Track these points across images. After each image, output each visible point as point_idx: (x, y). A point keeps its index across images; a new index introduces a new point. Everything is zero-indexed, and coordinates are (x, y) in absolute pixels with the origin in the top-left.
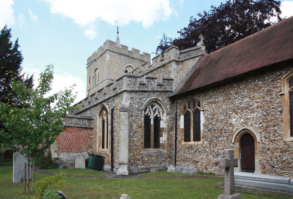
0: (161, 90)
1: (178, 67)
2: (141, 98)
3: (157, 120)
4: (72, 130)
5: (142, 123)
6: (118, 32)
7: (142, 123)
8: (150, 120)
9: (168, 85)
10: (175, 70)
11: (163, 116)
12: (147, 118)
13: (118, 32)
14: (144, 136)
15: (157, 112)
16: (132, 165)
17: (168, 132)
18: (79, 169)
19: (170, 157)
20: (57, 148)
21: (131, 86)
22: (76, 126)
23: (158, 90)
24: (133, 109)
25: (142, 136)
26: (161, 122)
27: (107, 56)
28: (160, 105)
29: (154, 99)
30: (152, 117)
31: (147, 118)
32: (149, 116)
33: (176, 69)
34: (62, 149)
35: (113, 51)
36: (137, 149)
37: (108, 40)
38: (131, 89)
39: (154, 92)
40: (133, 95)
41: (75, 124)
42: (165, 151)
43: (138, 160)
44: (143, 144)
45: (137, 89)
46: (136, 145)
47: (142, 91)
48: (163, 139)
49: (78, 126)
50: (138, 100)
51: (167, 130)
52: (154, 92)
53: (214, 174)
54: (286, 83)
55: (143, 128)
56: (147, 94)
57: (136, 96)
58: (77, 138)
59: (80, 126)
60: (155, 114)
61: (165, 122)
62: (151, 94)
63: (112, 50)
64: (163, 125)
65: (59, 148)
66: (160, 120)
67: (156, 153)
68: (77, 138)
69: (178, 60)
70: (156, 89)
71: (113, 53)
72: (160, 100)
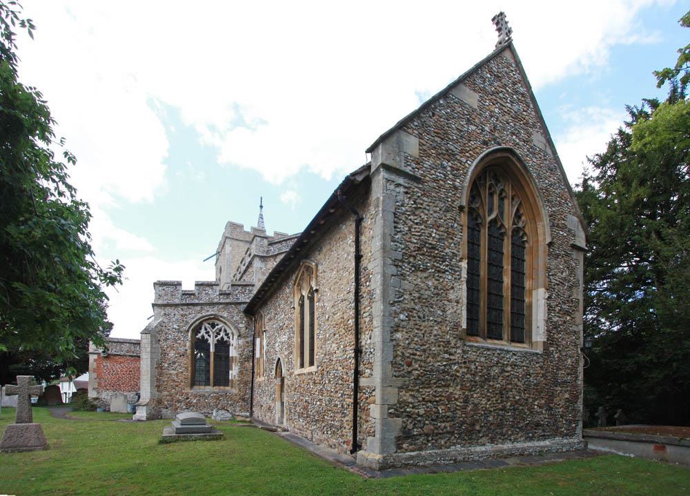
0: (228, 301)
1: (266, 265)
2: (185, 315)
3: (223, 346)
4: (122, 360)
5: (186, 350)
6: (261, 207)
7: (186, 350)
8: (209, 345)
9: (243, 293)
10: (258, 269)
11: (233, 339)
12: (201, 345)
13: (261, 207)
14: (190, 369)
15: (222, 334)
16: (167, 408)
17: (242, 364)
18: (115, 413)
19: (244, 400)
20: (97, 384)
21: (165, 298)
22: (129, 354)
23: (221, 301)
24: (168, 329)
25: (187, 368)
26: (231, 347)
27: (228, 248)
28: (225, 323)
29: (211, 315)
30: (212, 341)
31: (201, 345)
32: (207, 340)
33: (261, 269)
34: (106, 386)
35: (237, 238)
36: (177, 386)
37: (229, 222)
38: (165, 302)
39: (212, 304)
40: (169, 310)
41: (128, 351)
42: (235, 391)
43: (179, 401)
44: (189, 380)
45: (177, 301)
46: (174, 381)
47: (187, 305)
48: (234, 373)
49: (132, 354)
50: (178, 316)
51: (238, 359)
52: (212, 304)
53: (12, 407)
54: (296, 292)
55: (190, 357)
56: (198, 308)
57: (177, 313)
58: (131, 371)
59: (135, 354)
60: (219, 337)
61: (235, 348)
62: (206, 308)
63: (235, 237)
64: (233, 353)
65: (99, 384)
66: (229, 345)
67: (214, 393)
68: (131, 371)
69: (265, 255)
70: (216, 301)
71: (238, 242)
72: (225, 316)
